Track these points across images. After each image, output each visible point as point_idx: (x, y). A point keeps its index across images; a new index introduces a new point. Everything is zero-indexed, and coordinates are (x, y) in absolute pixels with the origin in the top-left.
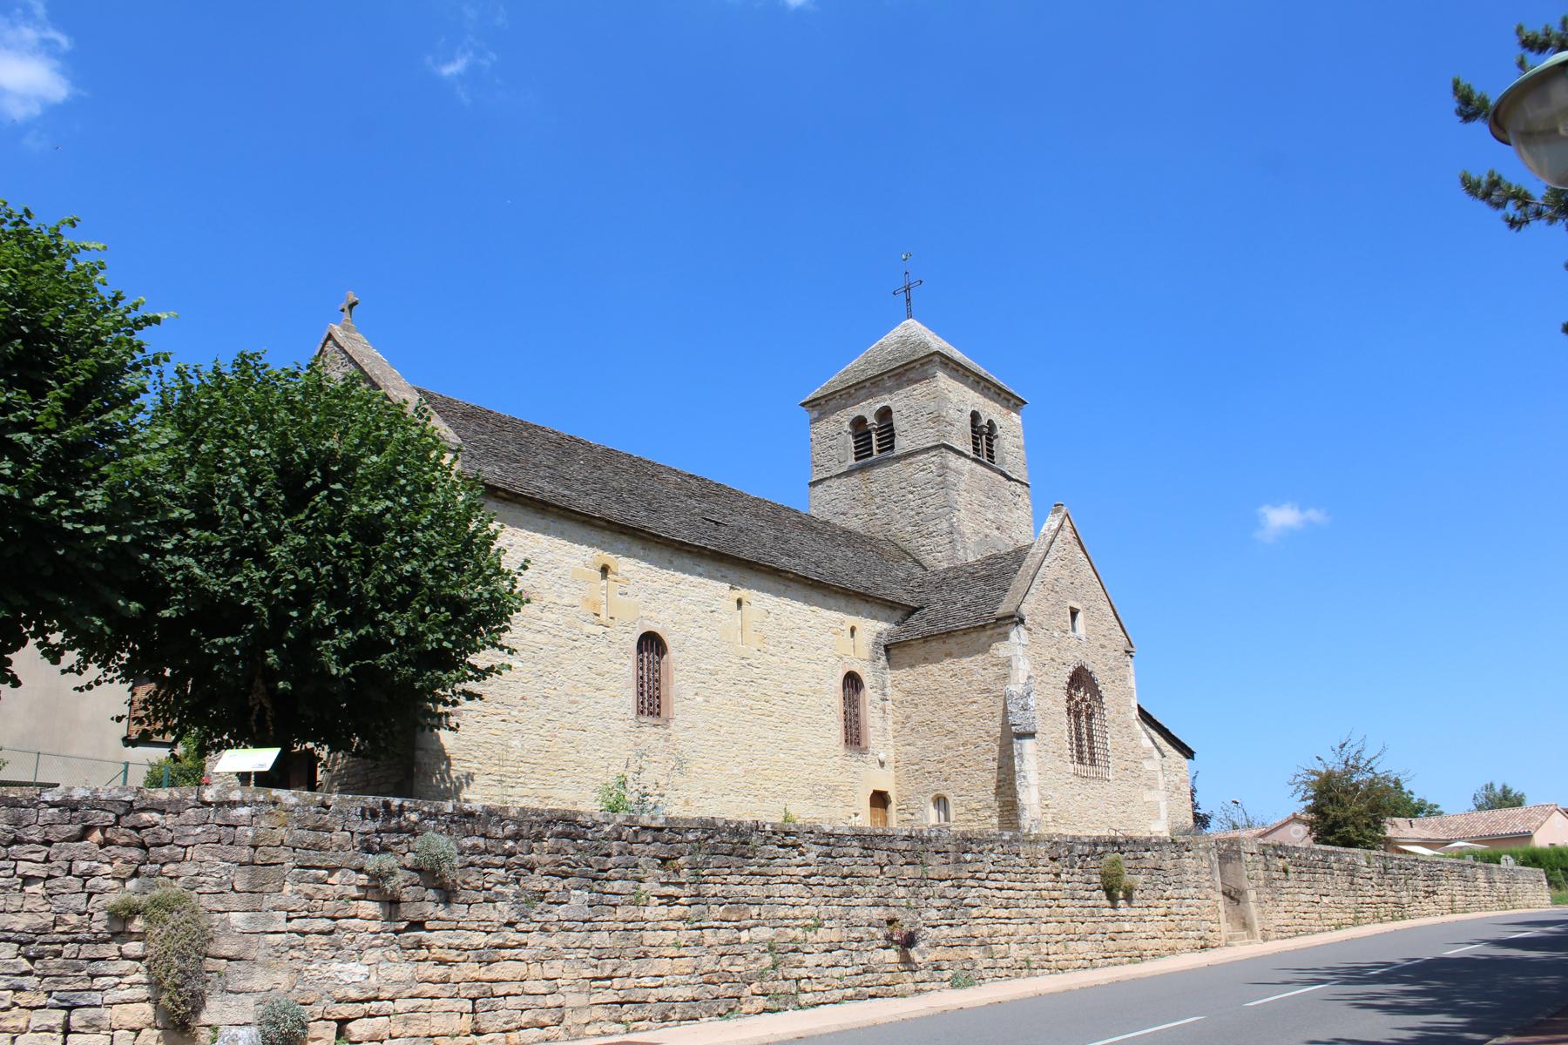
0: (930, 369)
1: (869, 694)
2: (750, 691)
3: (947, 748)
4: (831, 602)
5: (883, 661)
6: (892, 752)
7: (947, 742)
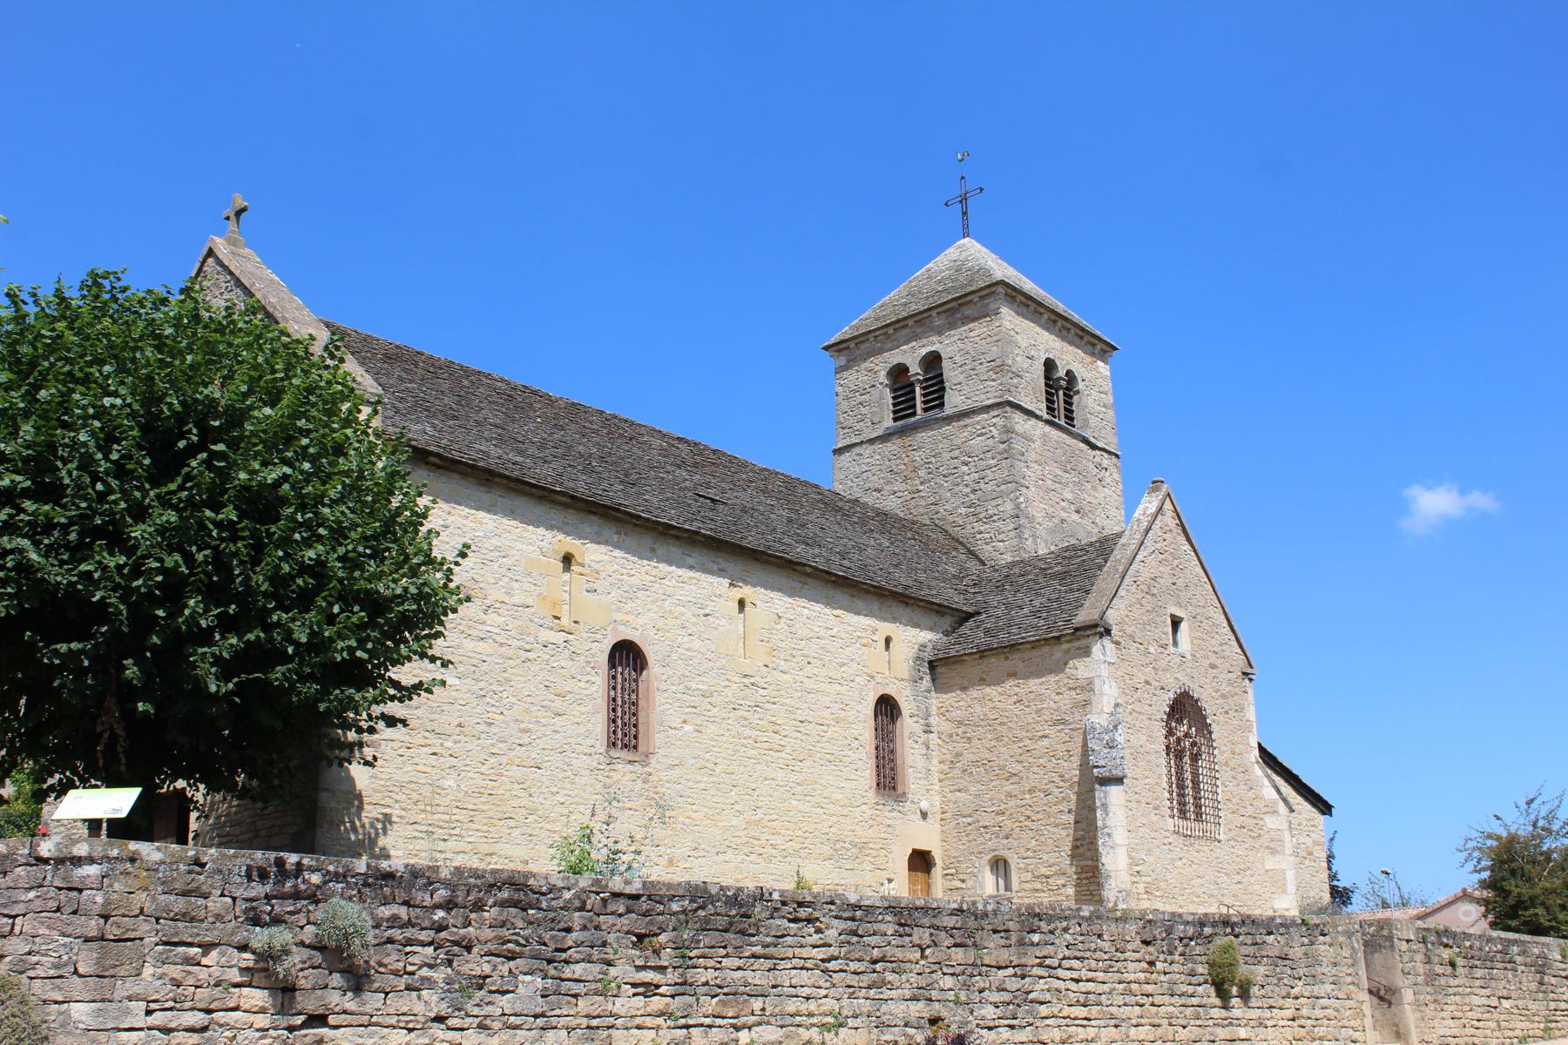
1: (908, 724)
3: (1010, 795)
5: (927, 682)
6: (937, 799)
7: (1009, 788)
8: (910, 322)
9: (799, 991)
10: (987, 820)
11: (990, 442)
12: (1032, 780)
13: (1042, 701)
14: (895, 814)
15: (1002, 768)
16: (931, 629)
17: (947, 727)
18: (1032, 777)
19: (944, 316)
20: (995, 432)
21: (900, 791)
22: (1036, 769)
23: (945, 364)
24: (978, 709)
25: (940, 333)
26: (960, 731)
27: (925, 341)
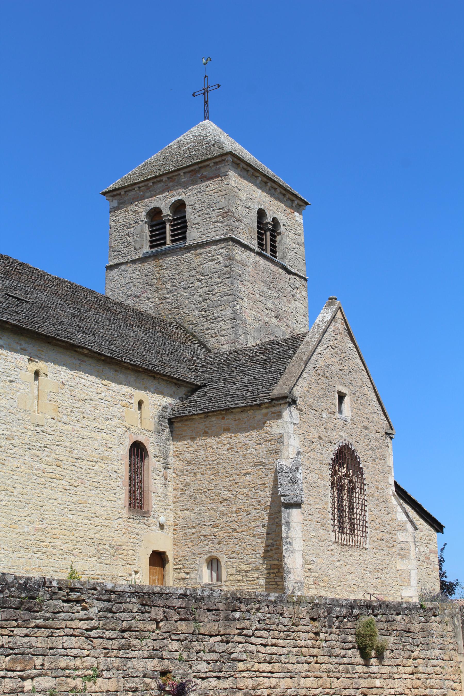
1: (153, 463)
3: (222, 514)
5: (166, 433)
6: (171, 516)
8: (165, 178)
10: (206, 531)
13: (247, 449)
14: (141, 526)
15: (217, 495)
19: (188, 175)
20: (221, 259)
21: (145, 509)
22: (241, 496)
23: (188, 209)
24: (202, 453)
26: (189, 468)
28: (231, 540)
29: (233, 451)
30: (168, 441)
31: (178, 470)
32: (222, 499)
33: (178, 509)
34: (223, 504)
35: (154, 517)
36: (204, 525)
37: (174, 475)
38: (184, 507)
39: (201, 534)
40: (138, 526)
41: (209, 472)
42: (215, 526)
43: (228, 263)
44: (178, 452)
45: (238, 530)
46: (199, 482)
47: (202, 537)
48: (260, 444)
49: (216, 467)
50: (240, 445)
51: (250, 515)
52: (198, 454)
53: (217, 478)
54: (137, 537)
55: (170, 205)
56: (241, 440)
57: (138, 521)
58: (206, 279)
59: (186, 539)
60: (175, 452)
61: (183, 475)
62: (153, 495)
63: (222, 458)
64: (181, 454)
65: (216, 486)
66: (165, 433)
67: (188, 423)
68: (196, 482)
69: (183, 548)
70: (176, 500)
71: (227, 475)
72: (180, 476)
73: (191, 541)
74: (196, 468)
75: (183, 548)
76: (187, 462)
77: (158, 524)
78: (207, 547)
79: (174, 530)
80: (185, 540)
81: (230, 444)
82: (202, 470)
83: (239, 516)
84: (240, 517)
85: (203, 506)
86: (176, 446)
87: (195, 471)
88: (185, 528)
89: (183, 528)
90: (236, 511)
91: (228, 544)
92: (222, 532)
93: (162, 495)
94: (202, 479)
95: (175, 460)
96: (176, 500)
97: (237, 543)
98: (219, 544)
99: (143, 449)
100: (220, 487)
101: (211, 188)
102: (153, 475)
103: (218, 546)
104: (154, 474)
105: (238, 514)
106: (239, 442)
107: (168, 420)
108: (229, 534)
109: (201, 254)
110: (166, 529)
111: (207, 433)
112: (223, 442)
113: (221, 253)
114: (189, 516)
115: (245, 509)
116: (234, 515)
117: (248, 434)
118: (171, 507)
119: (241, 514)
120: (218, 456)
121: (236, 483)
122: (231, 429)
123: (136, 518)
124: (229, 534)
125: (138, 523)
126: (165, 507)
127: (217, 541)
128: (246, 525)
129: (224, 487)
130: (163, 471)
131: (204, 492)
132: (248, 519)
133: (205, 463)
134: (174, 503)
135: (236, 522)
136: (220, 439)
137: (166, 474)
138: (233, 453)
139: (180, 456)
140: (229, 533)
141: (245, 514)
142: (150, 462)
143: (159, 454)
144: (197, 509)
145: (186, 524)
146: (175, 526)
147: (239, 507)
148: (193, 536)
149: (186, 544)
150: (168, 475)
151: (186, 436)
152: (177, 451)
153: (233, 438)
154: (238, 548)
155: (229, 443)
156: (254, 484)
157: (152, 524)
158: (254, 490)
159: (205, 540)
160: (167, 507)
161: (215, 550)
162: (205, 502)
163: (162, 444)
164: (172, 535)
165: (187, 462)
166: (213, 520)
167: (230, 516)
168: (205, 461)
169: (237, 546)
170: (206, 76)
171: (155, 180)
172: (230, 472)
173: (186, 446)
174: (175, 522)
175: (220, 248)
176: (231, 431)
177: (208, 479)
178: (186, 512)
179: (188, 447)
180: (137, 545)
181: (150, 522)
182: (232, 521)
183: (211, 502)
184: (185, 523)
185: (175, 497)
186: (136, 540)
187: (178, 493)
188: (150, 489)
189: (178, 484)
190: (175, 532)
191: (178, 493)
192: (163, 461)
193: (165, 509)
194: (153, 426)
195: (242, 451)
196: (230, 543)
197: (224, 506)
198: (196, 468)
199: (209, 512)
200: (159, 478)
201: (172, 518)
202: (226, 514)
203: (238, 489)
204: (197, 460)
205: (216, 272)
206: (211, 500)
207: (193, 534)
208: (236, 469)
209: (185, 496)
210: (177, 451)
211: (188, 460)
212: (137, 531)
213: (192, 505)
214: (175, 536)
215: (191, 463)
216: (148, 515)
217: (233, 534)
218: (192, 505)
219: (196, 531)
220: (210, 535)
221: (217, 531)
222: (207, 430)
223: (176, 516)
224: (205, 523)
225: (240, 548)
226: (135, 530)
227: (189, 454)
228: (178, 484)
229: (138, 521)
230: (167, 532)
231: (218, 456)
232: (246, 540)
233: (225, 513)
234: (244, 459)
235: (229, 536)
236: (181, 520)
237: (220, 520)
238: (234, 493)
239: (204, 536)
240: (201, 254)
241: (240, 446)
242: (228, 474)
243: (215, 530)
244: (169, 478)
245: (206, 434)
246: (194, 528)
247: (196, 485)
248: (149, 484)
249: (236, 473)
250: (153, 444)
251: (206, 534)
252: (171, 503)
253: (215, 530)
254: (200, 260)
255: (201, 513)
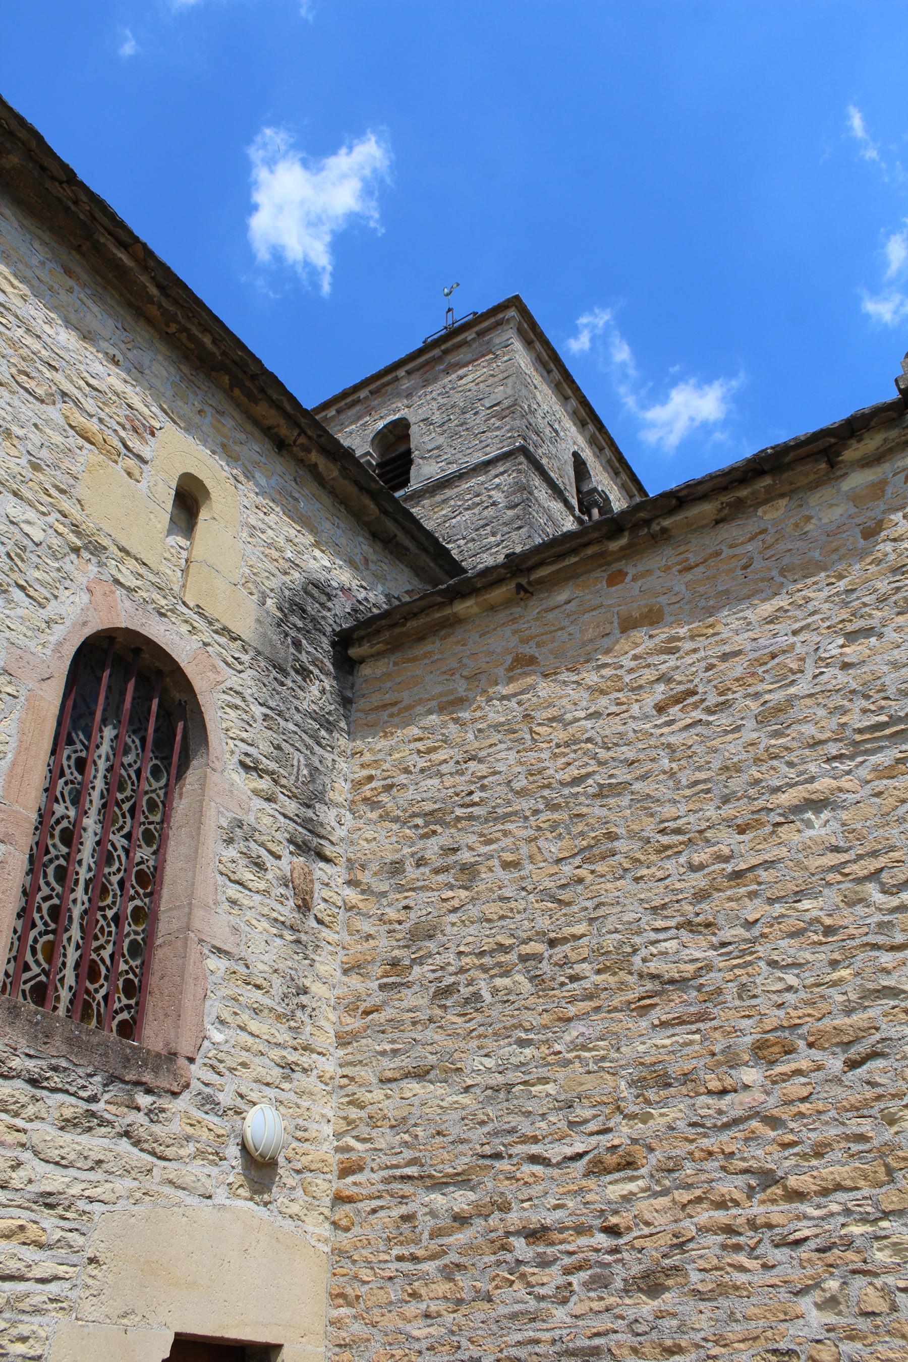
0: (498, 338)
1: (224, 791)
2: (68, 1215)
3: (656, 1079)
4: (97, 316)
5: (318, 693)
6: (325, 1115)
7: (647, 1042)
8: (363, 394)
9: (588, 1005)
10: (547, 1200)
11: (490, 512)
12: (776, 995)
13: (787, 678)
14: (95, 1143)
15: (614, 962)
16: (351, 563)
17: (377, 840)
18: (764, 978)
19: (417, 375)
20: (498, 496)
21: (153, 1036)
22: (788, 948)
23: (414, 430)
24: (507, 760)
25: (409, 396)
26: (432, 848)
27: (384, 411)
28: (741, 1258)
29: (695, 706)
30: (330, 731)
31: (375, 867)
32: (649, 986)
33: (366, 1074)
34: (656, 1015)
35: (208, 1103)
36: (534, 1159)
37: (352, 895)
38: (405, 1062)
39: (514, 1218)
40: (73, 1143)
41: (552, 847)
42: (611, 1160)
43: (516, 499)
44: (374, 784)
45: (793, 1182)
46: (493, 910)
47: (519, 1243)
48: (868, 632)
49: (598, 811)
50: (738, 668)
51: (880, 1063)
52: (483, 769)
53: (600, 868)
54: (49, 1224)
55: (372, 436)
56: (741, 641)
57: (72, 1107)
58: (459, 547)
59: (414, 1259)
60: (358, 784)
61: (400, 888)
62: (215, 963)
63: (631, 755)
64: (388, 788)
65: (600, 912)
66: (315, 689)
67: (432, 646)
68: (474, 911)
69: (390, 1321)
70: (354, 1023)
71: (665, 840)
72: (384, 894)
73: (448, 1273)
74: (472, 839)
75: (390, 1321)
76: (420, 821)
77: (233, 1151)
78: (560, 1314)
79: (340, 1199)
80: (407, 1266)
81: (669, 680)
82: (507, 842)
83: (786, 1077)
84: (796, 1087)
85: (523, 1043)
86: (368, 757)
87: (465, 856)
88: (407, 1188)
89: (396, 1186)
90: (759, 1048)
91: (723, 1290)
92: (664, 1201)
93: (277, 981)
94: (507, 892)
95: (360, 823)
96: (354, 1023)
97: (797, 1276)
98: (654, 1290)
99: (182, 706)
100: (629, 917)
101: (470, 378)
102: (218, 853)
103: (647, 1307)
104: (231, 852)
105: (779, 1069)
106: (725, 657)
107: (333, 644)
108: (721, 1217)
109: (444, 501)
110: (287, 1193)
111: (532, 661)
112: (627, 679)
113: (498, 485)
114: (432, 1112)
115: (827, 1024)
116: (751, 1075)
117: (781, 601)
118: (329, 1066)
119: (804, 1065)
120: (603, 754)
121: (737, 875)
122: (667, 610)
123: (57, 1080)
124: (721, 1217)
125: (67, 1124)
126: (292, 1057)
127: (636, 1270)
128: (861, 1138)
129: (654, 910)
130: (289, 863)
131: (524, 958)
132: (870, 1093)
133: (525, 805)
134: (344, 1040)
135: (773, 1122)
136: (606, 672)
137: (307, 875)
138: (697, 714)
139: (384, 798)
140: (721, 1205)
141: (835, 1064)
142: (214, 778)
143: (273, 766)
144: (479, 1062)
145: (413, 1162)
146: (345, 1172)
147: (776, 1017)
148: (461, 1237)
149: (414, 1295)
150: (319, 892)
151: (421, 701)
152: (370, 778)
153: (688, 645)
154: (816, 1319)
155: (664, 678)
156: (874, 854)
157: (191, 1148)
158: (878, 897)
159: (544, 1263)
160: (305, 1060)
161: (625, 1338)
162: (531, 1018)
163: (291, 726)
164: (326, 1230)
165: (420, 821)
166: (592, 1126)
167: (714, 1085)
168: (521, 793)
169: (806, 1304)
170: (450, 310)
171: (342, 404)
172: (692, 818)
173: (420, 745)
174: (348, 1149)
175: (496, 476)
176: (668, 619)
177: (548, 884)
178: (413, 1087)
179: (430, 751)
180: (40, 1294)
181: (177, 1127)
182: (736, 1122)
183: (572, 1010)
184: (408, 1154)
185: (351, 1009)
186: (30, 1254)
187: (365, 987)
188: (197, 924)
189: (369, 937)
190: (343, 1212)
191: (365, 987)
192: (292, 807)
193: (289, 1068)
194: (254, 625)
195: (757, 695)
196: (741, 1278)
197: (664, 1024)
198: (472, 839)
199: (561, 1074)
200: (262, 886)
201: (328, 1130)
202: (687, 1078)
203: (753, 910)
204: (476, 798)
205: (487, 525)
206: (573, 1000)
207: (462, 1220)
208: (726, 800)
209: (410, 998)
210: (370, 778)
211: (428, 807)
212: (56, 1180)
213: (450, 1044)
214: (344, 1240)
215: (442, 823)
216: (164, 1082)
217: (757, 1209)
218: (450, 1044)
219: (476, 1205)
220: (581, 1230)
221: (627, 1198)
222: (529, 650)
223: (354, 1113)
224: (535, 1149)
225: (830, 1318)
226: (33, 1167)
227: (436, 781)
228: (369, 937)
229: (72, 1107)
230: (295, 1208)
231: (603, 754)
232: (882, 1257)
233: (675, 1070)
234: (777, 734)
235: (729, 1230)
236: (384, 1138)
237: (646, 1118)
238: (726, 934)
239: (536, 1234)
240: (444, 501)
241: (738, 672)
242: (678, 831)
243: (615, 1191)
244: (319, 907)
245: (523, 663)
246: (462, 1180)
247: (472, 929)
248: (191, 896)
249: (728, 822)
250: (238, 701)
251: (550, 1218)
252: (326, 1040)
253: (615, 1191)
254: (444, 512)
255: (509, 1086)
